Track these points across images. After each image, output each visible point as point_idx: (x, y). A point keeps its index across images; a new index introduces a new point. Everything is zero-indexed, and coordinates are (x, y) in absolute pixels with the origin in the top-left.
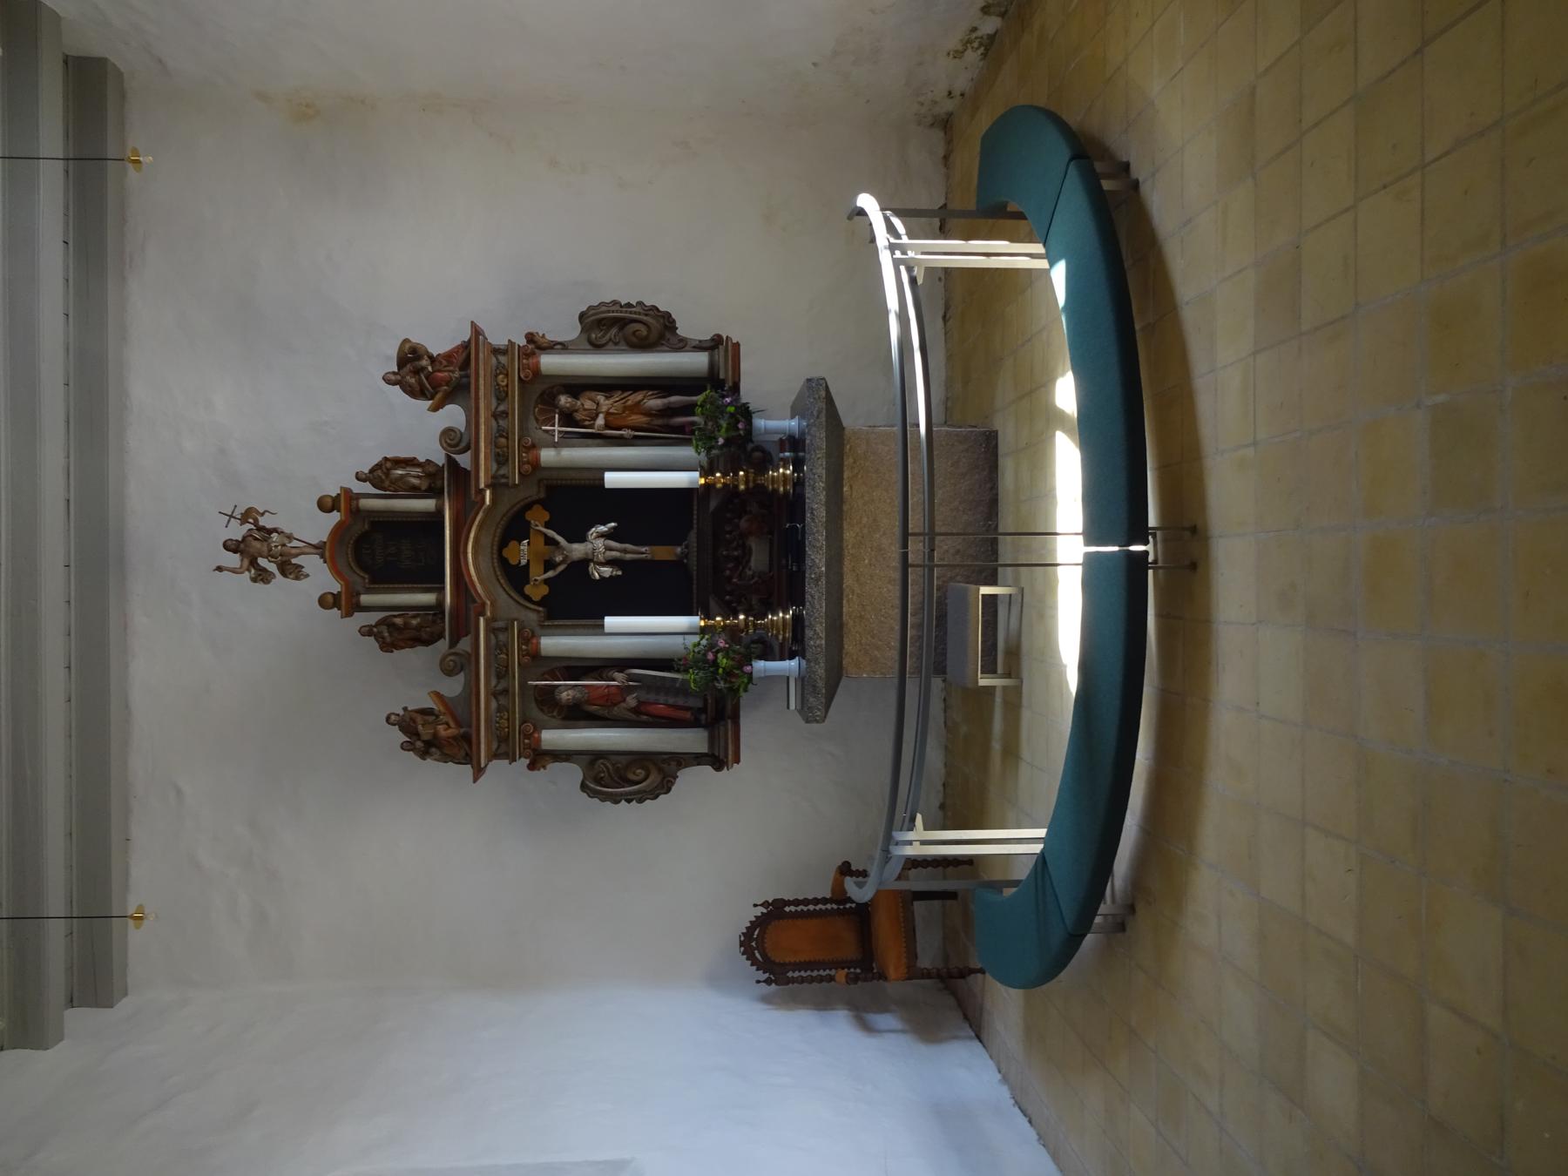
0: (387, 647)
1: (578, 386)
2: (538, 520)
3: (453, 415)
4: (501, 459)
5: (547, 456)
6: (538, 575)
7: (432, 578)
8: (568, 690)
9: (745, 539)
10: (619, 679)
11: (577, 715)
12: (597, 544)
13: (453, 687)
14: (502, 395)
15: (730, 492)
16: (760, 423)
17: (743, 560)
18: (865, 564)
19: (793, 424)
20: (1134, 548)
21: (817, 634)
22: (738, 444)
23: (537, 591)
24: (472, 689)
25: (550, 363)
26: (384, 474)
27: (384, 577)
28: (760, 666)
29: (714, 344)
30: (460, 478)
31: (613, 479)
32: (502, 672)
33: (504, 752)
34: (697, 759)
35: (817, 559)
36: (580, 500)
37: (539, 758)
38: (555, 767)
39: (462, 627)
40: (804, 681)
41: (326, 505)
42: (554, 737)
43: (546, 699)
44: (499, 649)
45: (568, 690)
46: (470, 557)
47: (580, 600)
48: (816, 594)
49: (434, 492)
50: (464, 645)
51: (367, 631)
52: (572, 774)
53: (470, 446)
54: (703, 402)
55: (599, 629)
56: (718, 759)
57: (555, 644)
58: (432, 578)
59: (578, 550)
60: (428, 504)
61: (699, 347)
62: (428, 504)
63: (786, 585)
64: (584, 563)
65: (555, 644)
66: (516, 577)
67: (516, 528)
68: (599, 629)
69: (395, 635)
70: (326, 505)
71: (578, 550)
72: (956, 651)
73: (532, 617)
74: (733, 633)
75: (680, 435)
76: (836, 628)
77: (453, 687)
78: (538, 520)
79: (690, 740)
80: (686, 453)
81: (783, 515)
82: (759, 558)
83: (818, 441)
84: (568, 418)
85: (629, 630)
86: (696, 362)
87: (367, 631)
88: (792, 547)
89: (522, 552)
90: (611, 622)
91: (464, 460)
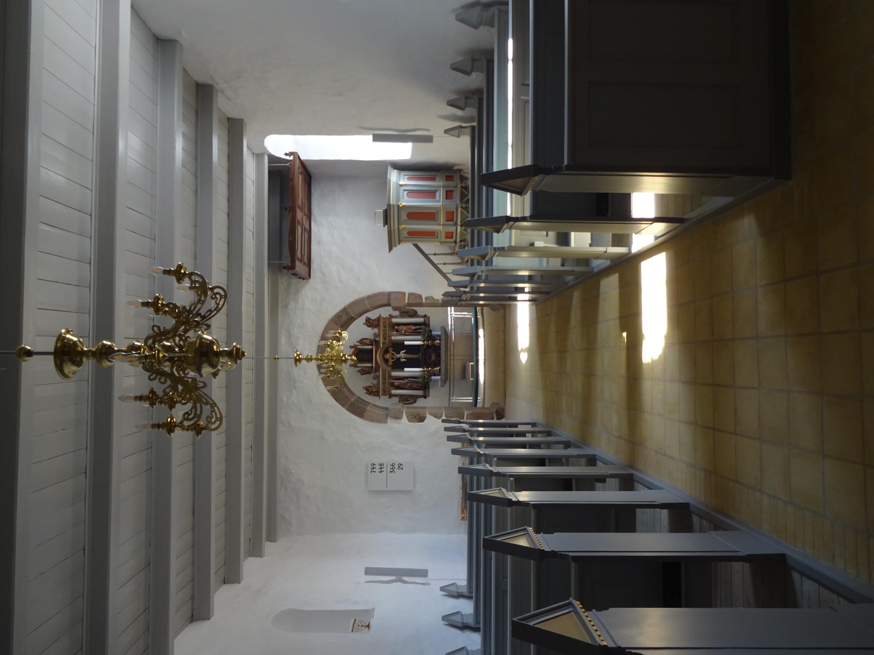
0: (362, 374)
1: (399, 324)
2: (391, 350)
3: (376, 330)
4: (385, 338)
5: (393, 338)
6: (391, 361)
7: (371, 361)
8: (397, 383)
9: (431, 353)
10: (406, 381)
11: (398, 387)
12: (402, 355)
13: (375, 382)
14: (385, 327)
15: (428, 345)
16: (433, 333)
17: (430, 358)
18: (455, 360)
19: (439, 333)
20: (109, 343)
21: (443, 371)
22: (430, 337)
23: (390, 363)
24: (379, 382)
25: (394, 320)
26: (362, 341)
27: (360, 360)
28: (433, 377)
29: (425, 316)
30: (377, 343)
31: (406, 343)
32: (384, 379)
33: (384, 394)
34: (421, 396)
35: (443, 358)
36: (399, 346)
37: (391, 396)
38: (394, 398)
39: (377, 369)
40: (441, 380)
41: (351, 347)
42: (394, 392)
43: (392, 385)
44: (384, 375)
45: (397, 383)
46: (378, 357)
47: (399, 365)
48: (443, 364)
49: (372, 345)
50: (377, 374)
51: (358, 371)
52: (396, 399)
53: (379, 335)
54: (423, 328)
55: (403, 371)
56: (425, 397)
57: (395, 374)
58: (371, 361)
59: (398, 356)
60: (370, 347)
61: (422, 317)
62: (370, 347)
63: (437, 363)
64: (400, 358)
65: (395, 374)
66: (386, 361)
67: (386, 351)
68: (403, 371)
69: (364, 372)
70: (351, 347)
71: (398, 356)
72: (468, 374)
73: (390, 369)
74: (428, 371)
75: (418, 334)
76: (446, 370)
77: (375, 382)
78: (391, 350)
79: (420, 393)
80: (419, 337)
81: (437, 349)
82: (433, 357)
83: (443, 337)
84: (397, 331)
85: (409, 371)
86: (421, 320)
87: (358, 371)
88: (439, 355)
89: (388, 356)
90: (406, 369)
91: (377, 339)
